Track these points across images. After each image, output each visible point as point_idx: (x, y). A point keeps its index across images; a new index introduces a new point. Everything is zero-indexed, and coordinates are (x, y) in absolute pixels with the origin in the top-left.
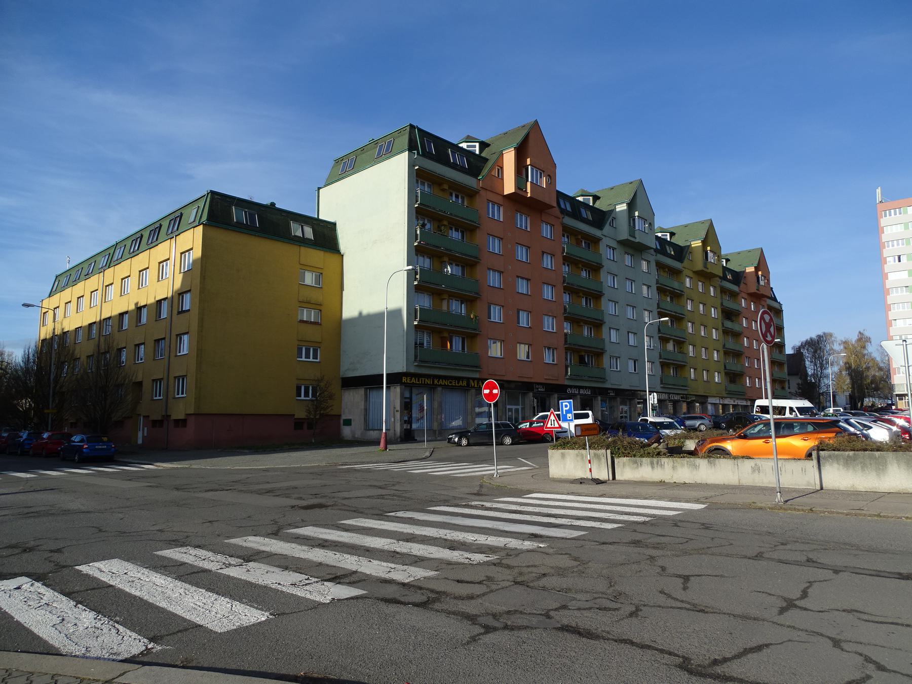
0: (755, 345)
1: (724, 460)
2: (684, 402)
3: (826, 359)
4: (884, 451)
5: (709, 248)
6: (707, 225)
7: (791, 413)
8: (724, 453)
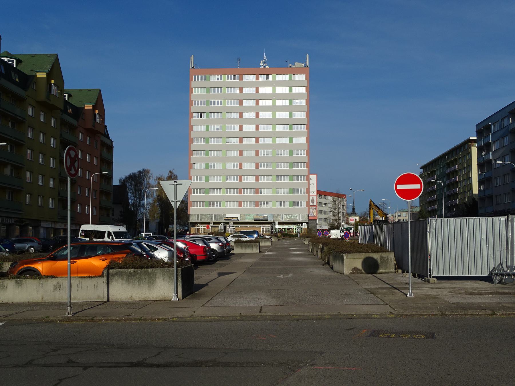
0: (87, 176)
1: (31, 280)
2: (17, 225)
3: (143, 192)
4: (156, 268)
5: (53, 81)
6: (53, 59)
7: (109, 237)
8: (35, 274)
